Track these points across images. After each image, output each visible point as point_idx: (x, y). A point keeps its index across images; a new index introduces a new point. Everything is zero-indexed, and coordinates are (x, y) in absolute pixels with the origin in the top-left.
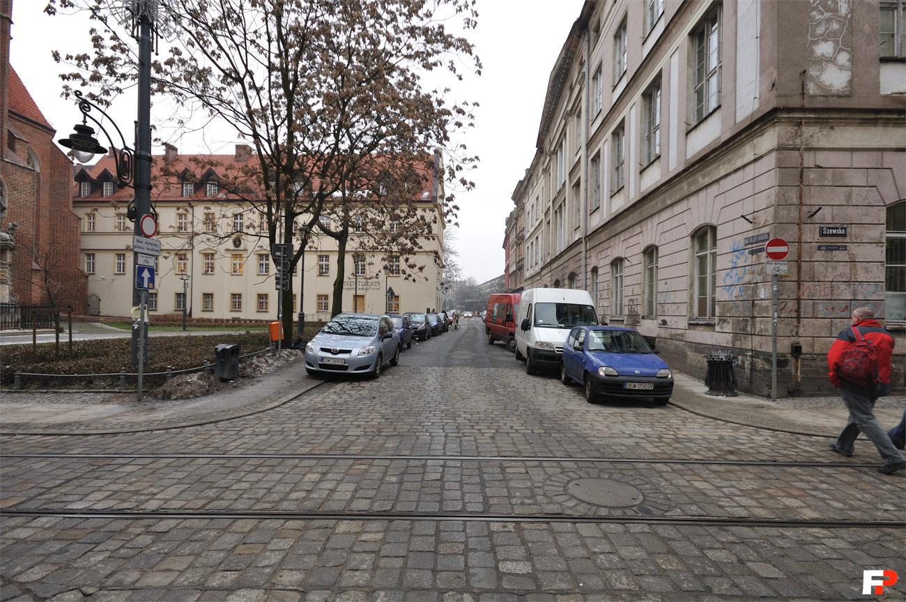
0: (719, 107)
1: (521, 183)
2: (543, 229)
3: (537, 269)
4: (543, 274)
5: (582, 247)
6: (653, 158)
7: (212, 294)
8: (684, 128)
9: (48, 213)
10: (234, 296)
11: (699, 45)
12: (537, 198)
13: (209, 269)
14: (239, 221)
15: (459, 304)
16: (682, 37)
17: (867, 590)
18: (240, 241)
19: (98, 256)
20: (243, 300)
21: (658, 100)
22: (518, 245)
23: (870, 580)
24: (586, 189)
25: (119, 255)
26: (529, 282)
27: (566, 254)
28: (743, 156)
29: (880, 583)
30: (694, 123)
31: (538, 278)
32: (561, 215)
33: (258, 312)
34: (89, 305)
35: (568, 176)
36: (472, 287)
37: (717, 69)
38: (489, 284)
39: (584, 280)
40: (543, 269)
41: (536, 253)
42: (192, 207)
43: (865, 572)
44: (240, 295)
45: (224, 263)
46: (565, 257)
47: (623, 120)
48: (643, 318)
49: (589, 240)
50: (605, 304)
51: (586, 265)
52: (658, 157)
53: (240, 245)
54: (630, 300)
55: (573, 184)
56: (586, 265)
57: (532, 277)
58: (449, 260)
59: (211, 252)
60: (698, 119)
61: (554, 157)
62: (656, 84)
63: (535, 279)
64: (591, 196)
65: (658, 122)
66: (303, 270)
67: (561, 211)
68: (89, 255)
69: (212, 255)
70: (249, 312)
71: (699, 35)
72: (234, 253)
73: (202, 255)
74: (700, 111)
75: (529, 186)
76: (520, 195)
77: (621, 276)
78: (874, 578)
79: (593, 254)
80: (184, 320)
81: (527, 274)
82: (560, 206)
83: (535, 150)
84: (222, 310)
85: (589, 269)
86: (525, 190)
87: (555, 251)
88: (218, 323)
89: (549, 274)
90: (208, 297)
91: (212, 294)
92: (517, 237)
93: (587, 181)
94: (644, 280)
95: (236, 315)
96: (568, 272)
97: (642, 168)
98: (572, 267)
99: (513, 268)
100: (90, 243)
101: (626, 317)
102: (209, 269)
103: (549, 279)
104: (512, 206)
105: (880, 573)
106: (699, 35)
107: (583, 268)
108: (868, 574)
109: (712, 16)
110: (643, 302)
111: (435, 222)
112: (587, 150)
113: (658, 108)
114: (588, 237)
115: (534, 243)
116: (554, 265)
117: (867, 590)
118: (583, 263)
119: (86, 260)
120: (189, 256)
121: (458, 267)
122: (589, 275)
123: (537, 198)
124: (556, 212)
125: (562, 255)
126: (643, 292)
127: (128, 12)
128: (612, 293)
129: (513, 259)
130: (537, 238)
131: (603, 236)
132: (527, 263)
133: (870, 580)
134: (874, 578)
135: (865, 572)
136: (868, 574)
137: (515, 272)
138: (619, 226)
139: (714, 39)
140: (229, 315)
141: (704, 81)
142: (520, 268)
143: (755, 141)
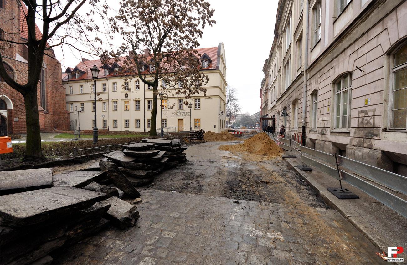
1: (267, 60)
2: (277, 81)
3: (274, 104)
4: (277, 105)
5: (304, 78)
7: (139, 120)
9: (51, 86)
10: (126, 120)
12: (275, 66)
13: (115, 108)
18: (127, 95)
19: (85, 104)
20: (130, 122)
22: (266, 93)
24: (308, 34)
25: (82, 104)
26: (271, 111)
27: (290, 88)
29: (395, 252)
31: (275, 108)
32: (288, 67)
33: (136, 128)
34: (71, 126)
35: (293, 37)
36: (248, 117)
39: (304, 102)
40: (277, 102)
41: (274, 95)
42: (108, 80)
44: (128, 120)
45: (121, 104)
46: (290, 91)
48: (385, 130)
49: (309, 72)
50: (325, 118)
51: (306, 92)
53: (127, 97)
54: (362, 112)
55: (296, 41)
56: (306, 92)
57: (272, 108)
58: (236, 104)
59: (116, 100)
61: (284, 34)
63: (274, 109)
64: (312, 37)
67: (288, 65)
68: (71, 104)
69: (116, 102)
70: (132, 128)
72: (125, 100)
73: (112, 102)
75: (271, 61)
76: (266, 69)
77: (351, 89)
78: (393, 250)
79: (313, 81)
80: (107, 132)
81: (270, 107)
82: (288, 62)
83: (273, 36)
84: (121, 128)
85: (309, 93)
86: (269, 64)
87: (284, 90)
88: (120, 133)
89: (280, 105)
90: (115, 121)
91: (139, 120)
92: (265, 89)
93: (308, 34)
94: (388, 87)
95: (127, 129)
96: (292, 99)
98: (295, 95)
99: (264, 105)
100: (71, 99)
101: (353, 131)
102: (115, 108)
103: (280, 107)
104: (263, 75)
105: (396, 248)
107: (304, 94)
110: (385, 111)
111: (104, 11)
112: (309, 4)
114: (309, 69)
115: (273, 90)
116: (283, 98)
118: (304, 90)
119: (70, 106)
120: (107, 103)
121: (240, 107)
122: (309, 98)
123: (275, 66)
124: (285, 67)
125: (288, 90)
126: (386, 101)
128: (333, 109)
129: (263, 101)
130: (274, 87)
131: (323, 63)
132: (270, 103)
134: (393, 250)
136: (390, 249)
137: (264, 107)
138: (345, 43)
140: (124, 130)
142: (266, 105)
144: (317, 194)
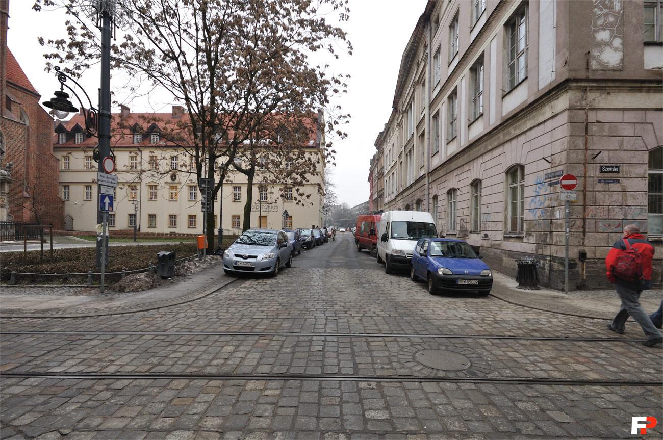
0: (526, 78)
1: (381, 133)
2: (397, 167)
3: (393, 196)
4: (397, 200)
5: (426, 180)
6: (478, 116)
7: (155, 215)
8: (500, 94)
9: (35, 156)
10: (171, 216)
11: (512, 33)
12: (393, 145)
13: (153, 197)
14: (175, 161)
15: (336, 222)
16: (499, 27)
17: (634, 432)
18: (175, 177)
19: (72, 187)
20: (178, 219)
21: (482, 73)
22: (379, 179)
23: (637, 424)
24: (429, 138)
25: (87, 187)
26: (387, 206)
27: (414, 185)
28: (543, 114)
29: (644, 426)
30: (508, 90)
31: (394, 203)
32: (410, 157)
33: (189, 228)
34: (65, 223)
35: (415, 129)
36: (345, 210)
37: (525, 51)
38: (358, 207)
39: (427, 204)
40: (397, 196)
41: (393, 185)
42: (141, 151)
43: (633, 418)
44: (176, 216)
45: (164, 192)
46: (414, 188)
47: (456, 88)
48: (471, 232)
49: (431, 175)
50: (443, 222)
51: (429, 194)
52: (482, 115)
53: (175, 179)
54: (461, 219)
55: (419, 135)
56: (429, 194)
57: (389, 202)
58: (328, 190)
59: (154, 184)
60: (511, 87)
61: (405, 114)
62: (480, 61)
63: (392, 204)
64: (433, 143)
65: (481, 89)
66: (222, 197)
67: (410, 155)
68: (65, 186)
69: (155, 186)
70: (182, 228)
71: (511, 25)
72: (171, 185)
73: (148, 187)
74: (512, 81)
75: (387, 136)
76: (380, 142)
77: (455, 202)
78: (640, 422)
79: (434, 185)
80: (135, 234)
81: (386, 200)
82: (410, 151)
83: (391, 109)
84: (163, 227)
85: (431, 196)
86: (384, 139)
87: (406, 183)
88: (159, 236)
89: (402, 201)
90: (152, 217)
91: (155, 215)
92: (378, 173)
93: (429, 132)
94: (472, 205)
95: (173, 230)
96: (416, 198)
97: (470, 123)
98: (418, 195)
99: (375, 196)
100: (66, 177)
101: (458, 232)
102: (153, 197)
103: (402, 204)
104: (374, 151)
105: (644, 419)
106: (511, 25)
107: (426, 196)
108: (635, 420)
109: (521, 12)
110: (470, 220)
111: (318, 162)
112: (430, 109)
113: (482, 79)
114: (431, 174)
115: (391, 178)
116: (406, 194)
117: (634, 432)
118: (427, 192)
119: (63, 190)
120: (138, 187)
121: (335, 195)
122: (431, 201)
123: (393, 145)
124: (407, 155)
125: (411, 186)
126: (471, 214)
127: (94, 9)
128: (448, 214)
129: (375, 189)
130: (393, 174)
131: (441, 173)
132: (386, 192)
133: (637, 424)
134: (640, 422)
135: (633, 418)
136: (635, 420)
137: (377, 199)
138: (453, 165)
139: (522, 28)
140: (167, 231)
141: (515, 60)
142: (381, 196)
143: (552, 103)
144: (420, 229)
